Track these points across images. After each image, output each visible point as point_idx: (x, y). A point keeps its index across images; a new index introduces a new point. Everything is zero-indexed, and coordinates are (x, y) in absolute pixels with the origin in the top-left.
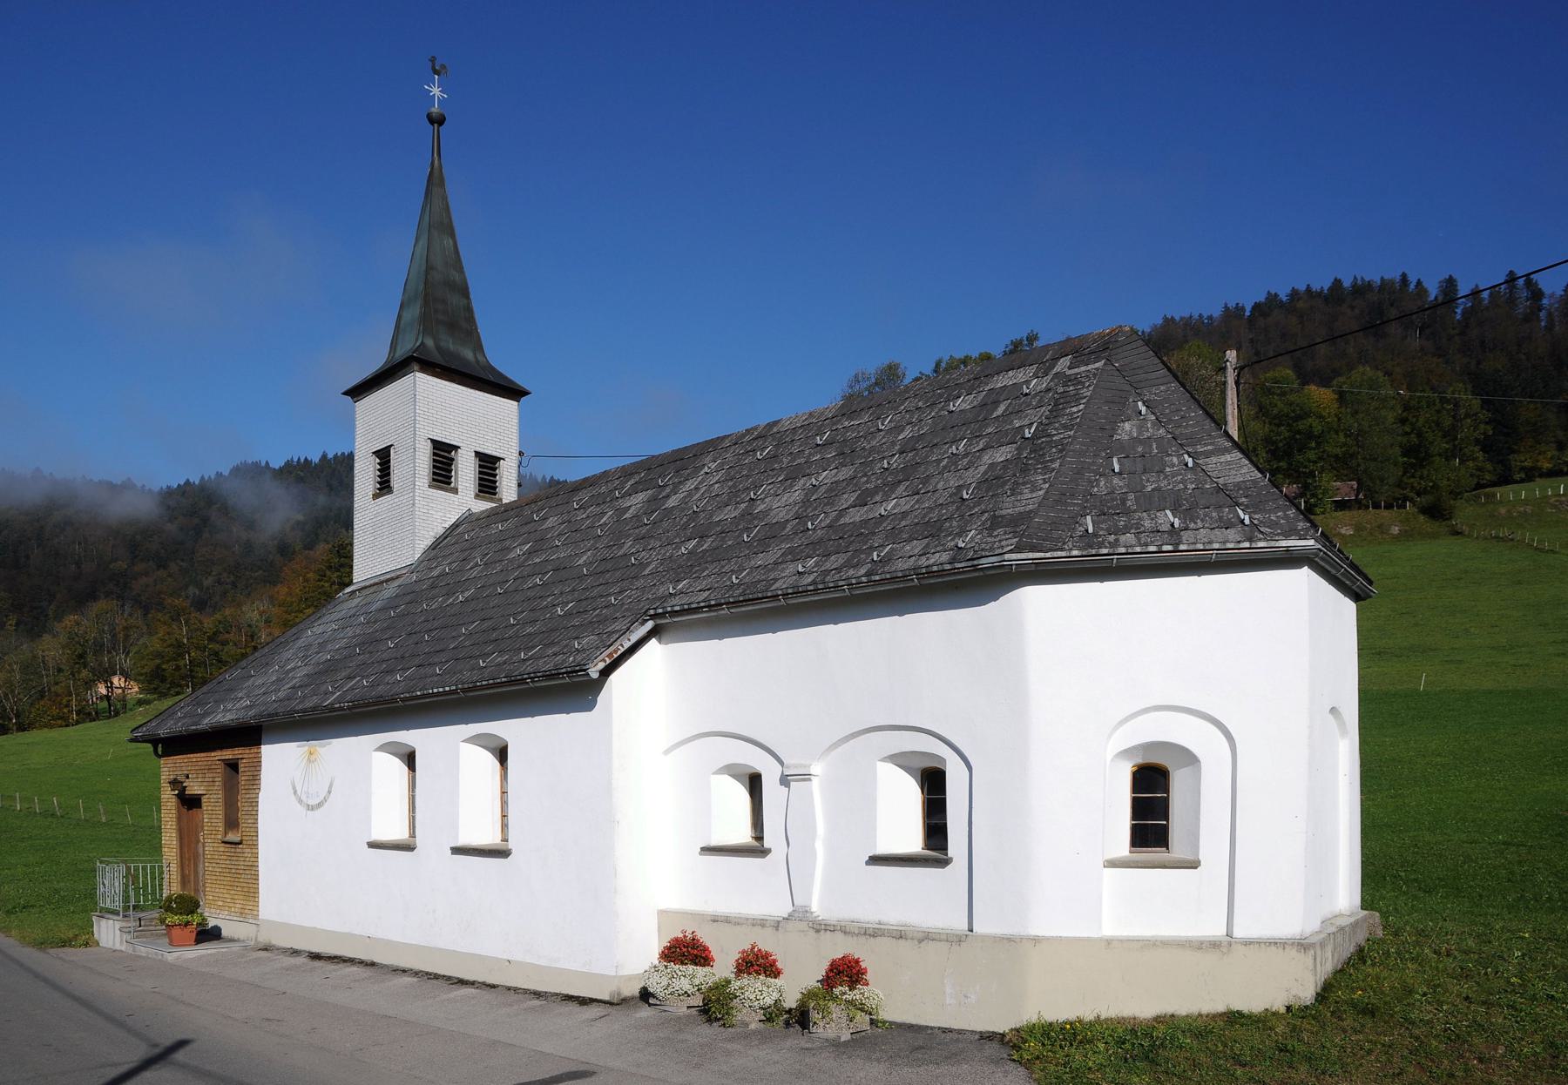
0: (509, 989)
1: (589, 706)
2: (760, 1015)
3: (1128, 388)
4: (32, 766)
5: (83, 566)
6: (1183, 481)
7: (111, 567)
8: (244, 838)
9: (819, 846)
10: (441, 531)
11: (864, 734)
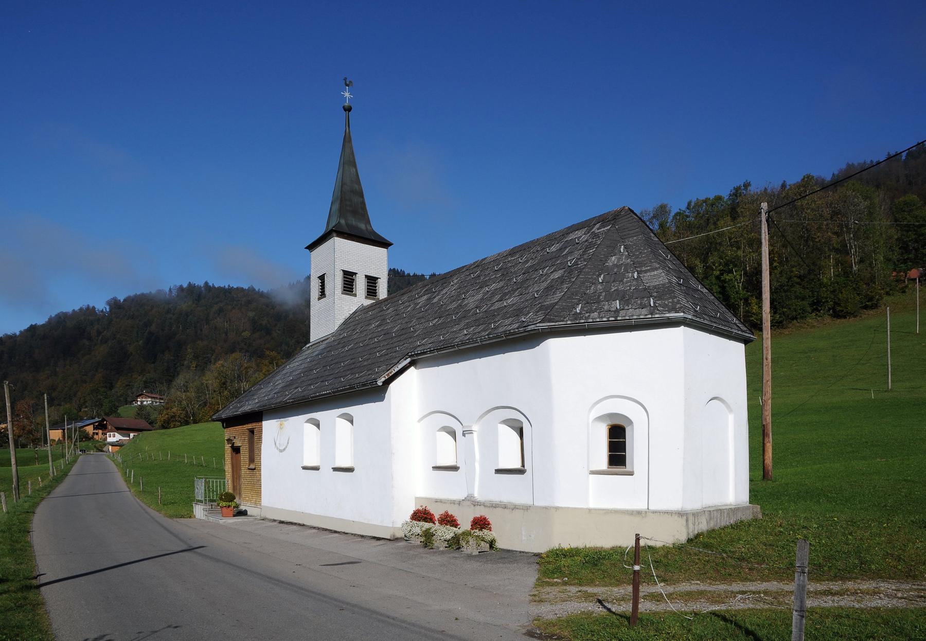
0: (352, 534)
1: (382, 399)
2: (446, 544)
3: (619, 239)
4: (196, 441)
5: (229, 334)
6: (630, 286)
7: (242, 334)
8: (257, 467)
9: (477, 465)
10: (348, 315)
11: (492, 411)
